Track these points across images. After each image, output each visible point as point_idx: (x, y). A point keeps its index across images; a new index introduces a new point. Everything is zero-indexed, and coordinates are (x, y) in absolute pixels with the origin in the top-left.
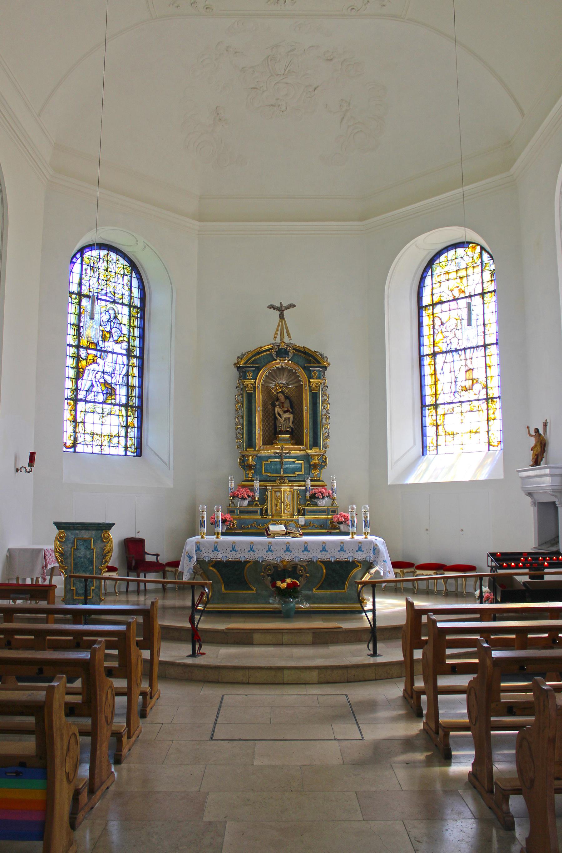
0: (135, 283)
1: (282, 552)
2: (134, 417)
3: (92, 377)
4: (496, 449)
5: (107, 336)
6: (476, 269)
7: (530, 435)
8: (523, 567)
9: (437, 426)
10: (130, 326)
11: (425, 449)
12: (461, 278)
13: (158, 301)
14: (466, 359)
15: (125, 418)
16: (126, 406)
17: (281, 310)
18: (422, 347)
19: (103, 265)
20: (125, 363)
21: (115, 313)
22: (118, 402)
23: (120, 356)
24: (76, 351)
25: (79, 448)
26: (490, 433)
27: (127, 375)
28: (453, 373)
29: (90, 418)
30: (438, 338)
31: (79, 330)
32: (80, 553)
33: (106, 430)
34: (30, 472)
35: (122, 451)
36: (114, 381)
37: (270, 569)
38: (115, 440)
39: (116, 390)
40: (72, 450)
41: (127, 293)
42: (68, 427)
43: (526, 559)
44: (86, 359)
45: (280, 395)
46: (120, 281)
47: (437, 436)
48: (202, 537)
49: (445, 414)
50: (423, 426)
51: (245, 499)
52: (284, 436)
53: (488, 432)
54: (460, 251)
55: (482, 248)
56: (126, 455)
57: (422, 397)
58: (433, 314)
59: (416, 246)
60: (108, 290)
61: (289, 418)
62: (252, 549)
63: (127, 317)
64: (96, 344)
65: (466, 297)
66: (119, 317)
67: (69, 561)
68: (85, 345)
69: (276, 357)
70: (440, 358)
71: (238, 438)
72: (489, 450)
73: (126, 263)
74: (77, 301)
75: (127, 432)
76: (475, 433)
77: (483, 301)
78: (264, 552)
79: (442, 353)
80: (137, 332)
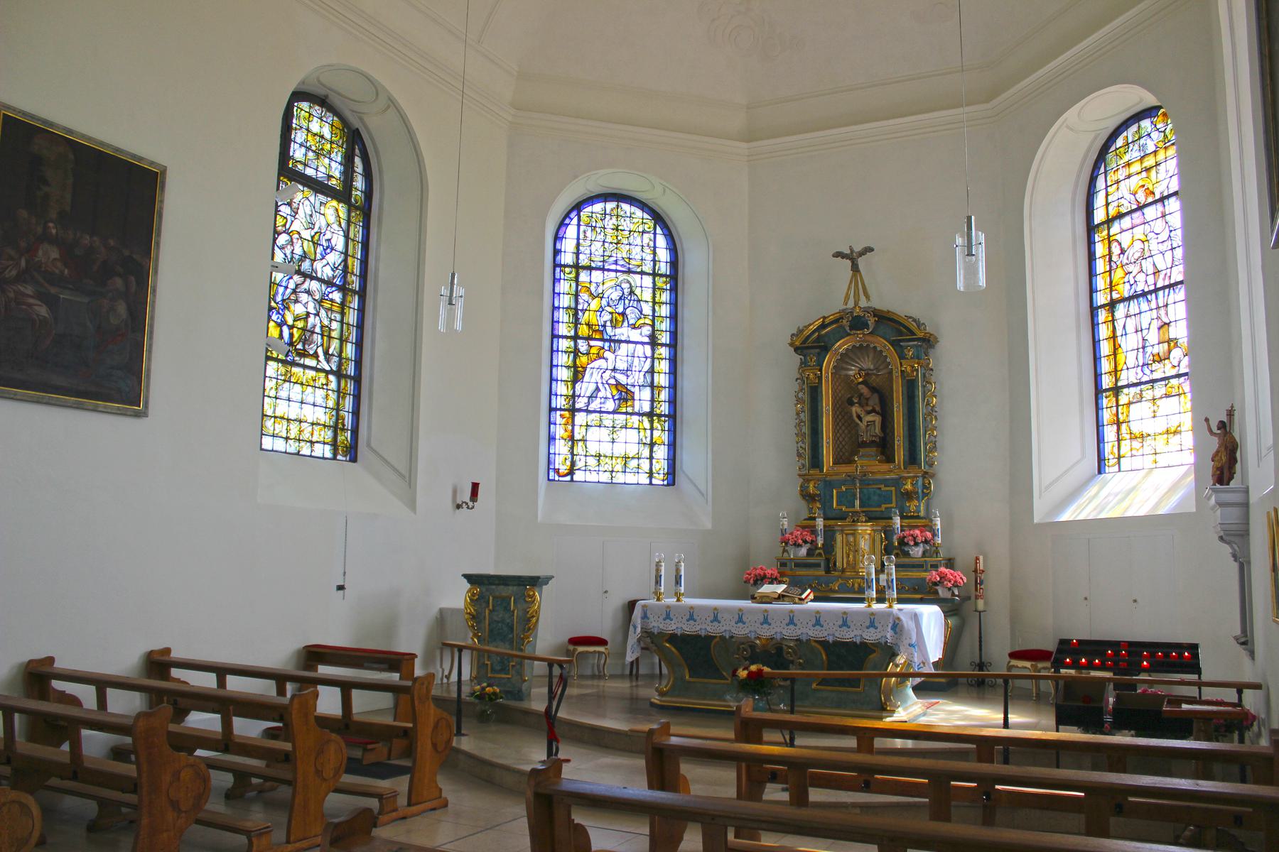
0: (661, 241)
3: (596, 377)
10: (654, 303)
12: (1148, 170)
15: (648, 432)
16: (650, 415)
17: (853, 258)
19: (610, 223)
21: (631, 287)
22: (636, 410)
23: (639, 346)
24: (572, 344)
25: (578, 476)
27: (652, 371)
29: (593, 434)
31: (576, 315)
33: (619, 450)
35: (644, 479)
36: (630, 381)
38: (633, 464)
40: (568, 478)
41: (650, 257)
42: (561, 448)
43: (1117, 653)
44: (588, 354)
45: (860, 387)
46: (638, 241)
47: (1119, 440)
49: (1130, 403)
50: (1099, 426)
51: (799, 546)
54: (1146, 124)
56: (651, 483)
57: (1097, 377)
59: (1067, 127)
63: (650, 291)
65: (1155, 202)
66: (638, 291)
68: (586, 335)
70: (1121, 310)
71: (799, 455)
73: (646, 216)
74: (573, 275)
75: (651, 451)
78: (733, 623)
80: (664, 311)
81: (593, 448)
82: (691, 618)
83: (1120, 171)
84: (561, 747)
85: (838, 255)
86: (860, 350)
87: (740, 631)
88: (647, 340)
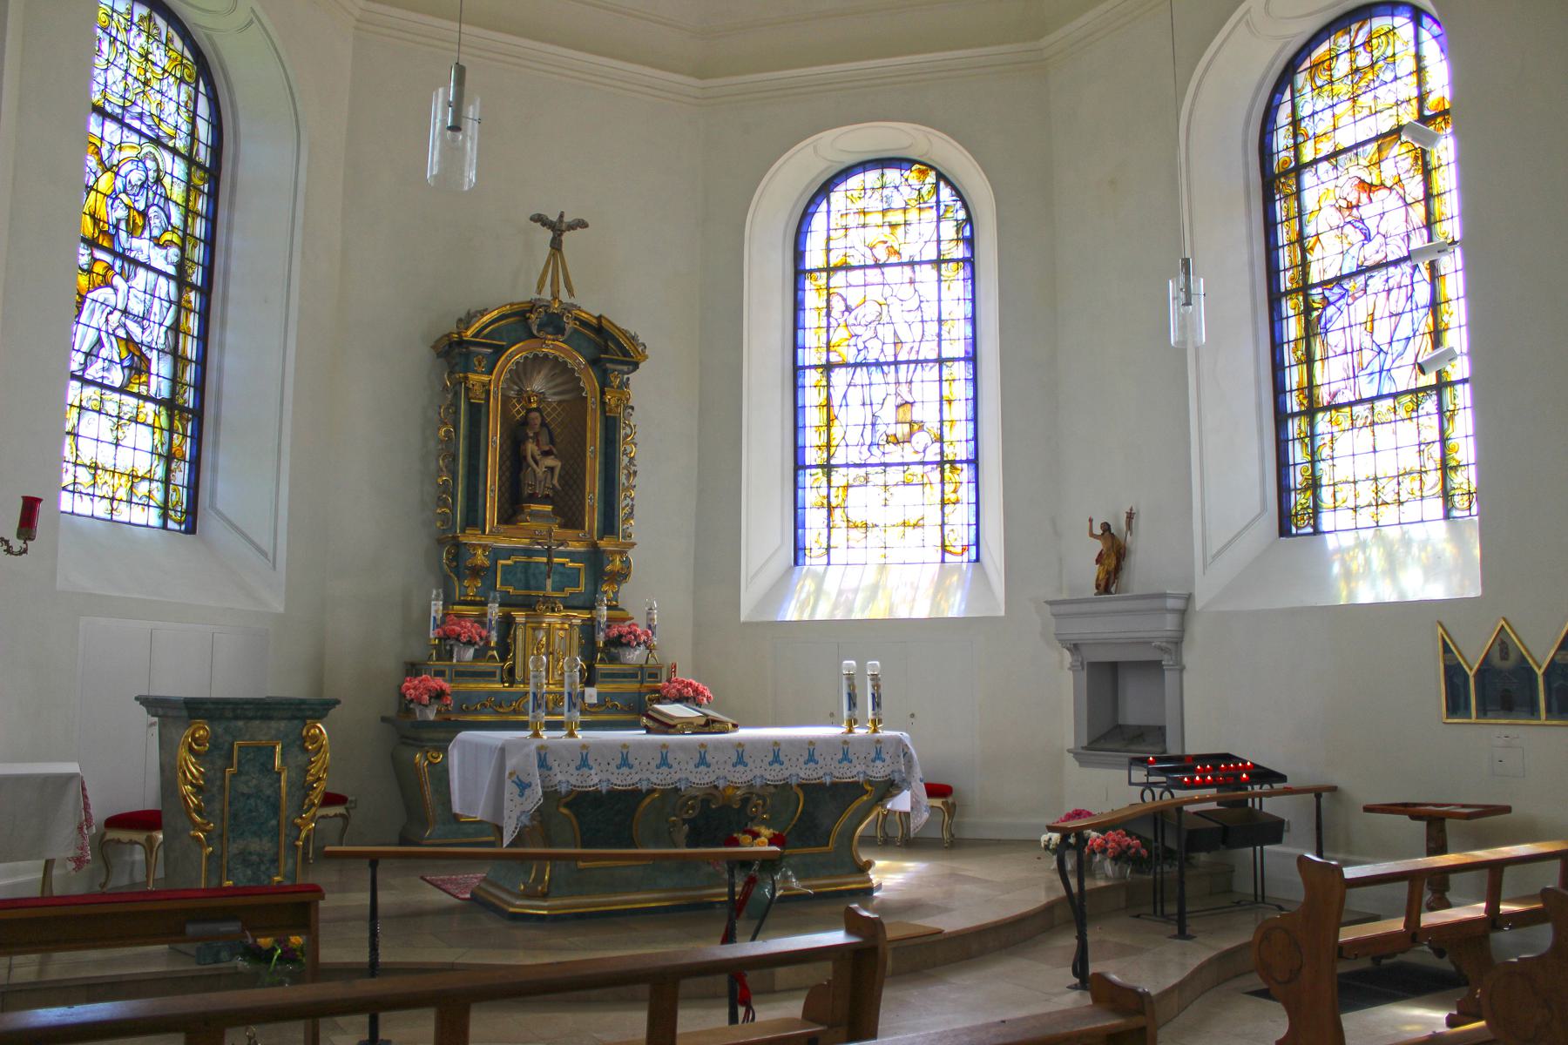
0: (203, 108)
1: (729, 767)
2: (185, 436)
4: (959, 559)
5: (138, 223)
6: (924, 214)
7: (1092, 535)
8: (1204, 785)
9: (830, 509)
11: (801, 554)
12: (891, 225)
13: (260, 160)
14: (898, 383)
15: (166, 434)
17: (558, 229)
18: (800, 351)
20: (173, 298)
21: (158, 170)
22: (152, 393)
26: (947, 528)
27: (176, 328)
28: (868, 408)
30: (839, 335)
32: (246, 783)
33: (125, 460)
34: (20, 553)
35: (154, 517)
36: (146, 339)
37: (693, 807)
38: (143, 488)
39: (150, 361)
41: (185, 128)
44: (90, 272)
46: (173, 93)
47: (829, 527)
48: (571, 734)
49: (848, 487)
52: (535, 507)
53: (943, 525)
54: (892, 175)
55: (940, 176)
56: (165, 526)
57: (798, 450)
58: (828, 288)
60: (146, 107)
61: (552, 469)
62: (664, 762)
64: (113, 237)
65: (902, 264)
66: (167, 180)
67: (217, 806)
69: (541, 327)
70: (839, 376)
72: (943, 561)
73: (187, 53)
75: (168, 471)
76: (915, 526)
77: (940, 275)
78: (691, 766)
79: (847, 365)
80: (199, 228)
81: (88, 452)
82: (625, 762)
83: (851, 217)
84: (755, 1007)
85: (539, 219)
86: (536, 362)
87: (660, 778)
88: (171, 270)
